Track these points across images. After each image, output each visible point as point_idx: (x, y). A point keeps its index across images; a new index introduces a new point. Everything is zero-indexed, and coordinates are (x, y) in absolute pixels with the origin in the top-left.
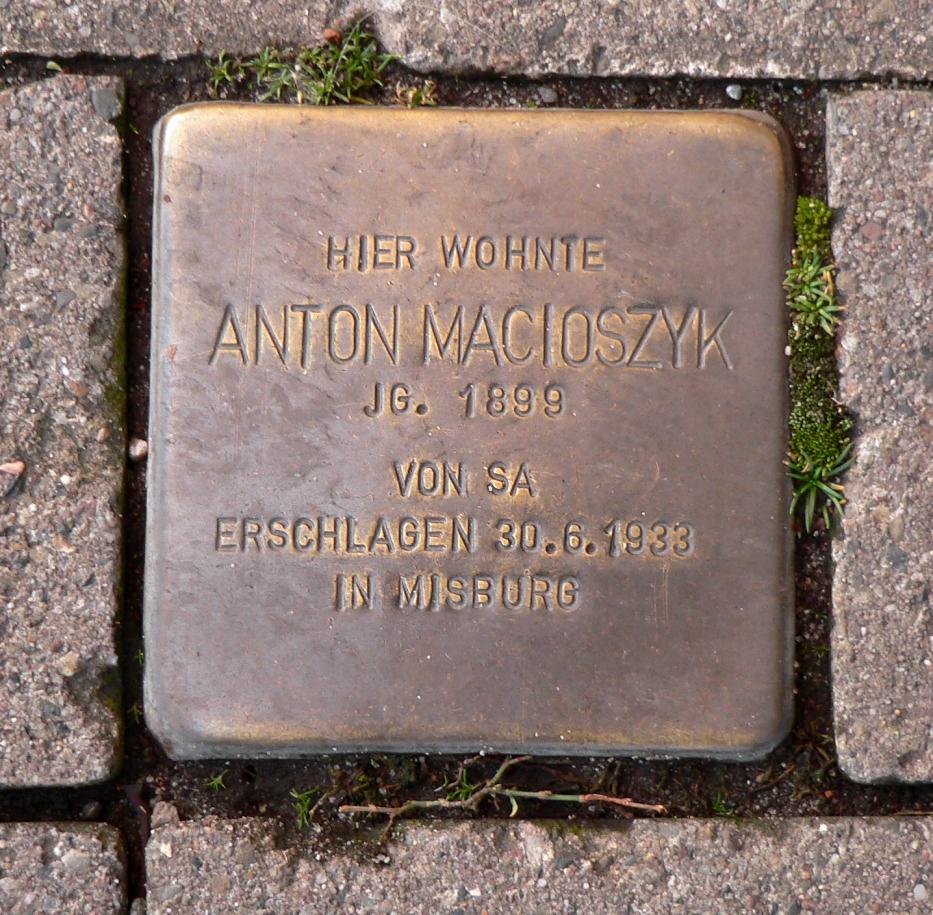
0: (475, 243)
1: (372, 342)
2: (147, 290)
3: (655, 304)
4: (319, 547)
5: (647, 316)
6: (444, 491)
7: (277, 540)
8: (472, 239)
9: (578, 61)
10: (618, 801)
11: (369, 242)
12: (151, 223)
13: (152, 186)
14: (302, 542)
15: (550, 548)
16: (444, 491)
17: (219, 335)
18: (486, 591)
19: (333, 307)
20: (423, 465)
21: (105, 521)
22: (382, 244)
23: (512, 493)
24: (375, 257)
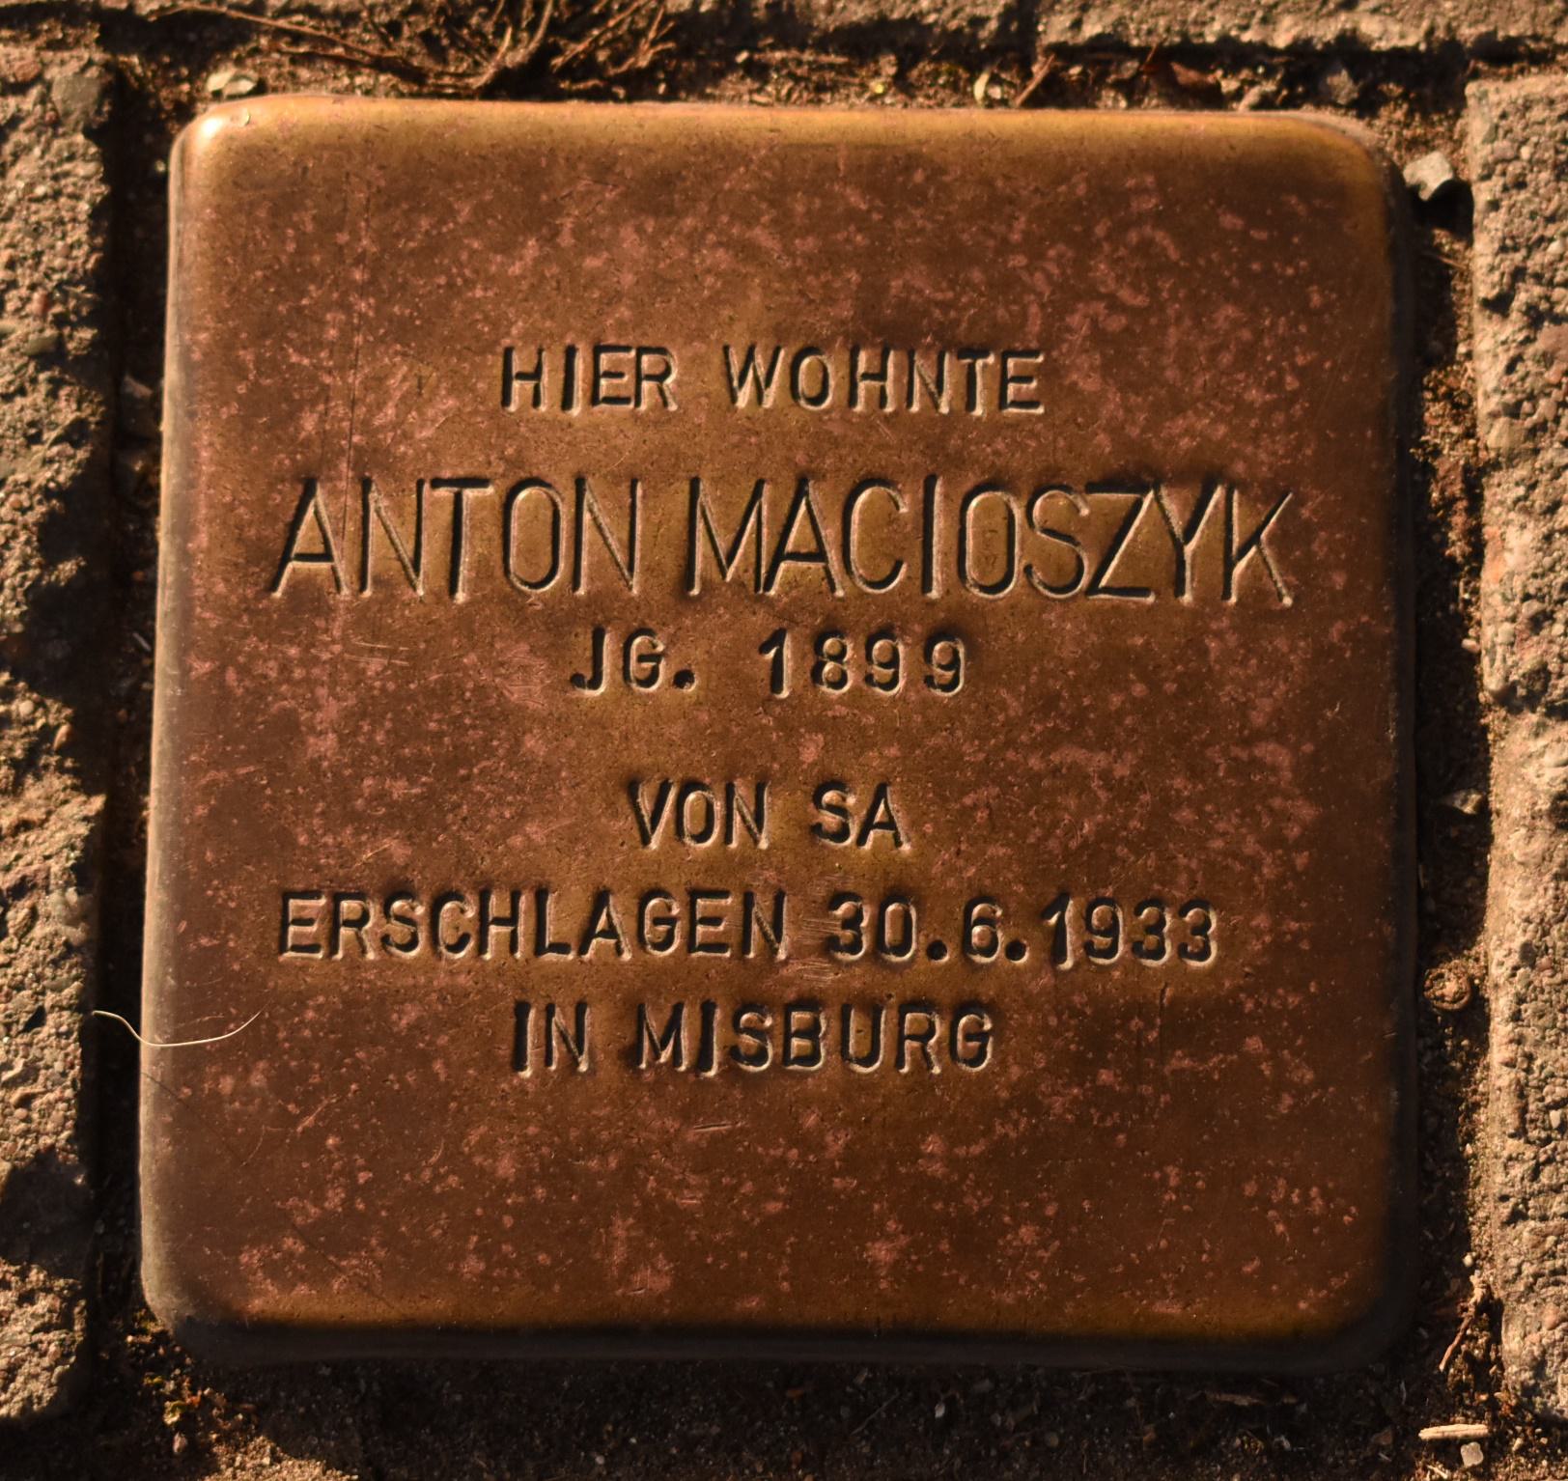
0: (790, 360)
1: (586, 537)
2: (161, 168)
3: (1136, 478)
4: (482, 948)
5: (1122, 498)
6: (727, 837)
7: (398, 931)
8: (782, 353)
9: (987, 19)
10: (1121, 936)
11: (580, 366)
12: (151, 639)
13: (151, 561)
14: (447, 935)
15: (935, 950)
16: (727, 837)
17: (291, 540)
18: (811, 1032)
19: (510, 482)
20: (688, 787)
21: (66, 904)
22: (605, 360)
23: (861, 839)
24: (596, 385)
